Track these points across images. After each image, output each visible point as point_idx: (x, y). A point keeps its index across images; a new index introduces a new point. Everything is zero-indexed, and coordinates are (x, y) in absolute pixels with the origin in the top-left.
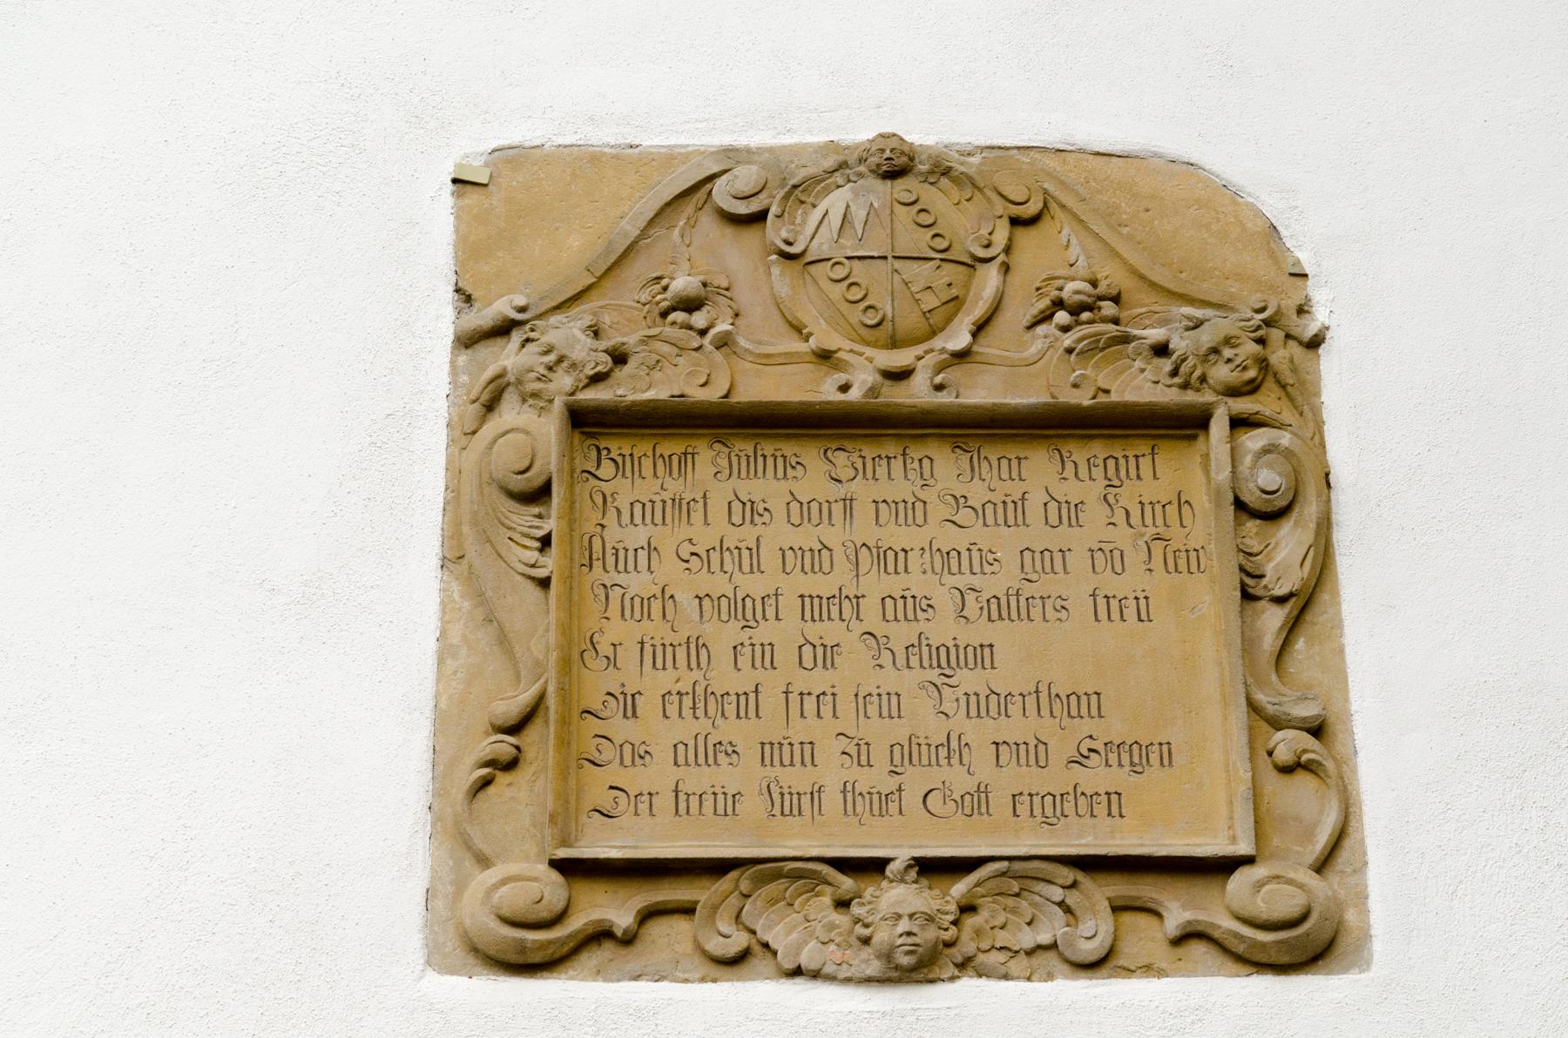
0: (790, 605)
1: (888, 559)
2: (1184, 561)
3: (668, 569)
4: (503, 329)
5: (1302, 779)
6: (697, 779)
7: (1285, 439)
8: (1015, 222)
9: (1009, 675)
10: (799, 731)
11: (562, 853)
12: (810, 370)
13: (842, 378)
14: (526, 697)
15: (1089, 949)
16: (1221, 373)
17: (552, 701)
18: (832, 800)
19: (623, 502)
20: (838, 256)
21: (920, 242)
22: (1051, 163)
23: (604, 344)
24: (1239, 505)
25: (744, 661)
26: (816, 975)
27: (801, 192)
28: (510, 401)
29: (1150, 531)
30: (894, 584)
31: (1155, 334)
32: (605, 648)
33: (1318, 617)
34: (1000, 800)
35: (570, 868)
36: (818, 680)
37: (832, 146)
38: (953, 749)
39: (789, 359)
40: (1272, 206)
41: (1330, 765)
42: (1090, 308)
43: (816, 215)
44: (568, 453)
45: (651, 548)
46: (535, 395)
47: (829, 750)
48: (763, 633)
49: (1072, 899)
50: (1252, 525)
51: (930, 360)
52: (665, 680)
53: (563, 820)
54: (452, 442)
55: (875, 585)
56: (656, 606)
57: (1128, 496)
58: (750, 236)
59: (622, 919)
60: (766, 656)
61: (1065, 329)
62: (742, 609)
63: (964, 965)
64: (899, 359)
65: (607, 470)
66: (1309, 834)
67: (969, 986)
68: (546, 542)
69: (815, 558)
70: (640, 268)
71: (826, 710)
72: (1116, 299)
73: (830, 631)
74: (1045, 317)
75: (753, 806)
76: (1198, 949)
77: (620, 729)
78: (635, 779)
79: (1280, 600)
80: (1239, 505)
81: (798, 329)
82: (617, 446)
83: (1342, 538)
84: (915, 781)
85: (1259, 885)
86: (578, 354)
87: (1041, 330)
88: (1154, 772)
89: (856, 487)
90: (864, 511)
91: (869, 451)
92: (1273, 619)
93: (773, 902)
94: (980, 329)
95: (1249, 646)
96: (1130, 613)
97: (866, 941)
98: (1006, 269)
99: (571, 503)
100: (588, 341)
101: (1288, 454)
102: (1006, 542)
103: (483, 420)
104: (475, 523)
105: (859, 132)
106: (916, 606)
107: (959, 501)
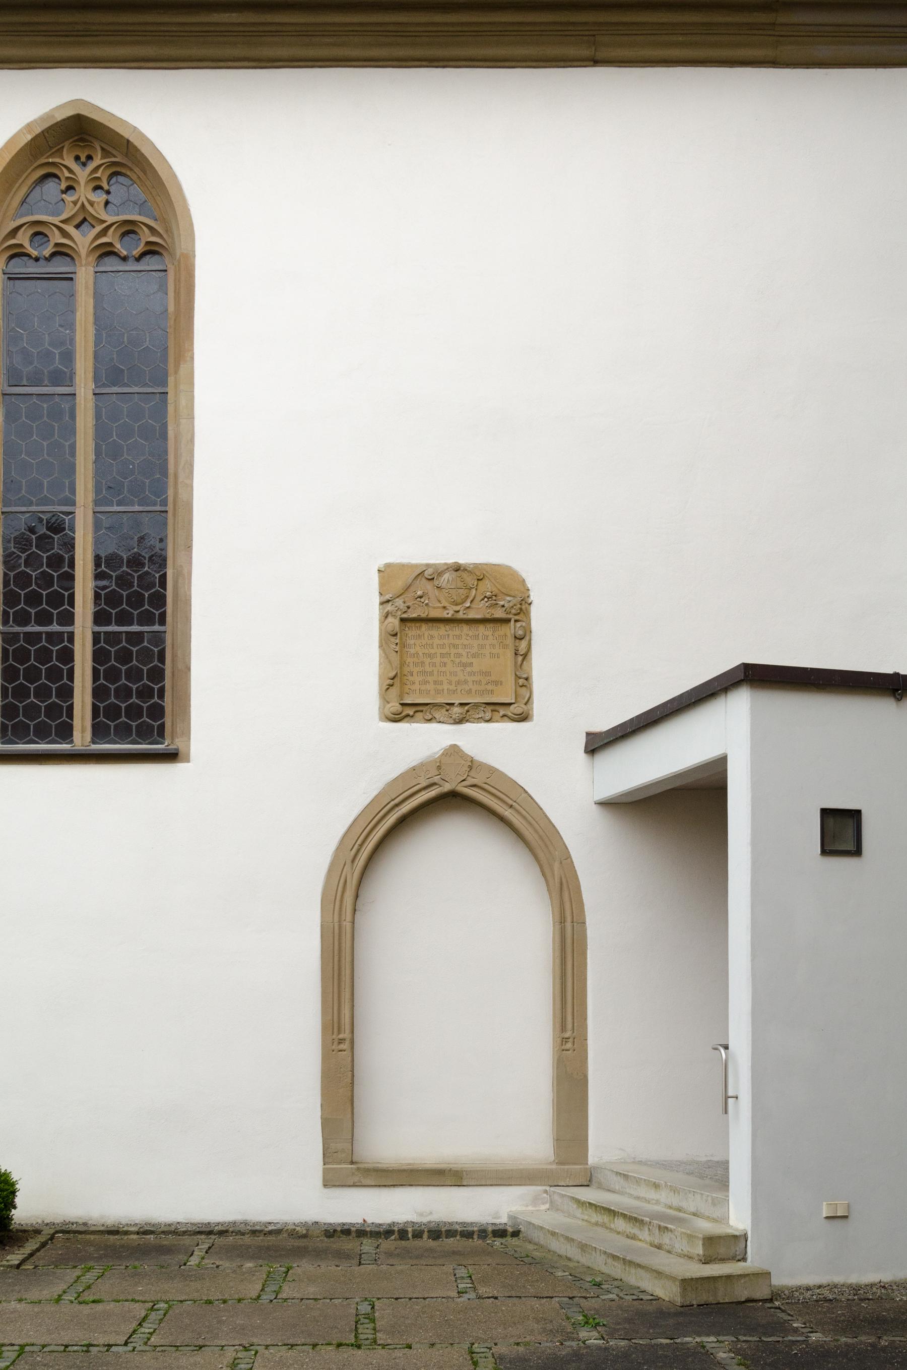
0: (438, 655)
1: (455, 646)
2: (505, 647)
3: (418, 648)
4: (388, 601)
5: (524, 688)
6: (423, 687)
7: (524, 624)
8: (478, 580)
9: (475, 668)
10: (440, 679)
11: (401, 702)
12: (440, 610)
13: (447, 611)
14: (394, 673)
15: (487, 718)
16: (513, 611)
17: (399, 674)
18: (445, 691)
19: (410, 635)
20: (447, 587)
21: (460, 584)
22: (485, 566)
23: (407, 605)
24: (515, 637)
25: (431, 666)
26: (443, 723)
27: (440, 574)
28: (390, 617)
29: (500, 641)
30: (456, 651)
31: (502, 603)
32: (407, 663)
33: (528, 657)
34: (473, 691)
35: (401, 704)
36: (443, 669)
37: (446, 564)
38: (466, 682)
39: (438, 607)
40: (524, 575)
41: (528, 686)
42: (491, 598)
43: (443, 578)
44: (400, 627)
45: (415, 644)
46: (394, 616)
47: (445, 682)
48: (434, 660)
49: (485, 710)
50: (517, 641)
51: (463, 608)
52: (418, 669)
53: (401, 696)
54: (380, 623)
55: (453, 651)
56: (416, 655)
57: (496, 634)
58: (431, 582)
59: (411, 713)
60: (434, 665)
61: (486, 602)
62: (430, 656)
63: (467, 721)
64: (457, 608)
65: (407, 629)
66: (524, 698)
67: (468, 724)
68: (397, 644)
69: (443, 646)
70: (412, 589)
71: (445, 675)
72: (496, 596)
73: (445, 660)
74: (483, 599)
75: (432, 692)
76: (506, 718)
77: (411, 678)
78: (413, 687)
79: (522, 655)
80: (515, 637)
81: (439, 601)
82: (409, 624)
83: (533, 642)
84: (459, 688)
85: (515, 708)
86: (401, 607)
87: (482, 602)
88: (499, 686)
89: (450, 632)
90: (451, 637)
91: (452, 625)
92: (520, 658)
93: (436, 710)
94: (472, 602)
95: (516, 663)
96: (496, 656)
97: (451, 717)
98: (476, 589)
99: (401, 636)
100: (402, 604)
101: (524, 627)
102: (475, 643)
103: (385, 620)
104: (384, 640)
105: (451, 561)
106: (459, 655)
107: (467, 635)
